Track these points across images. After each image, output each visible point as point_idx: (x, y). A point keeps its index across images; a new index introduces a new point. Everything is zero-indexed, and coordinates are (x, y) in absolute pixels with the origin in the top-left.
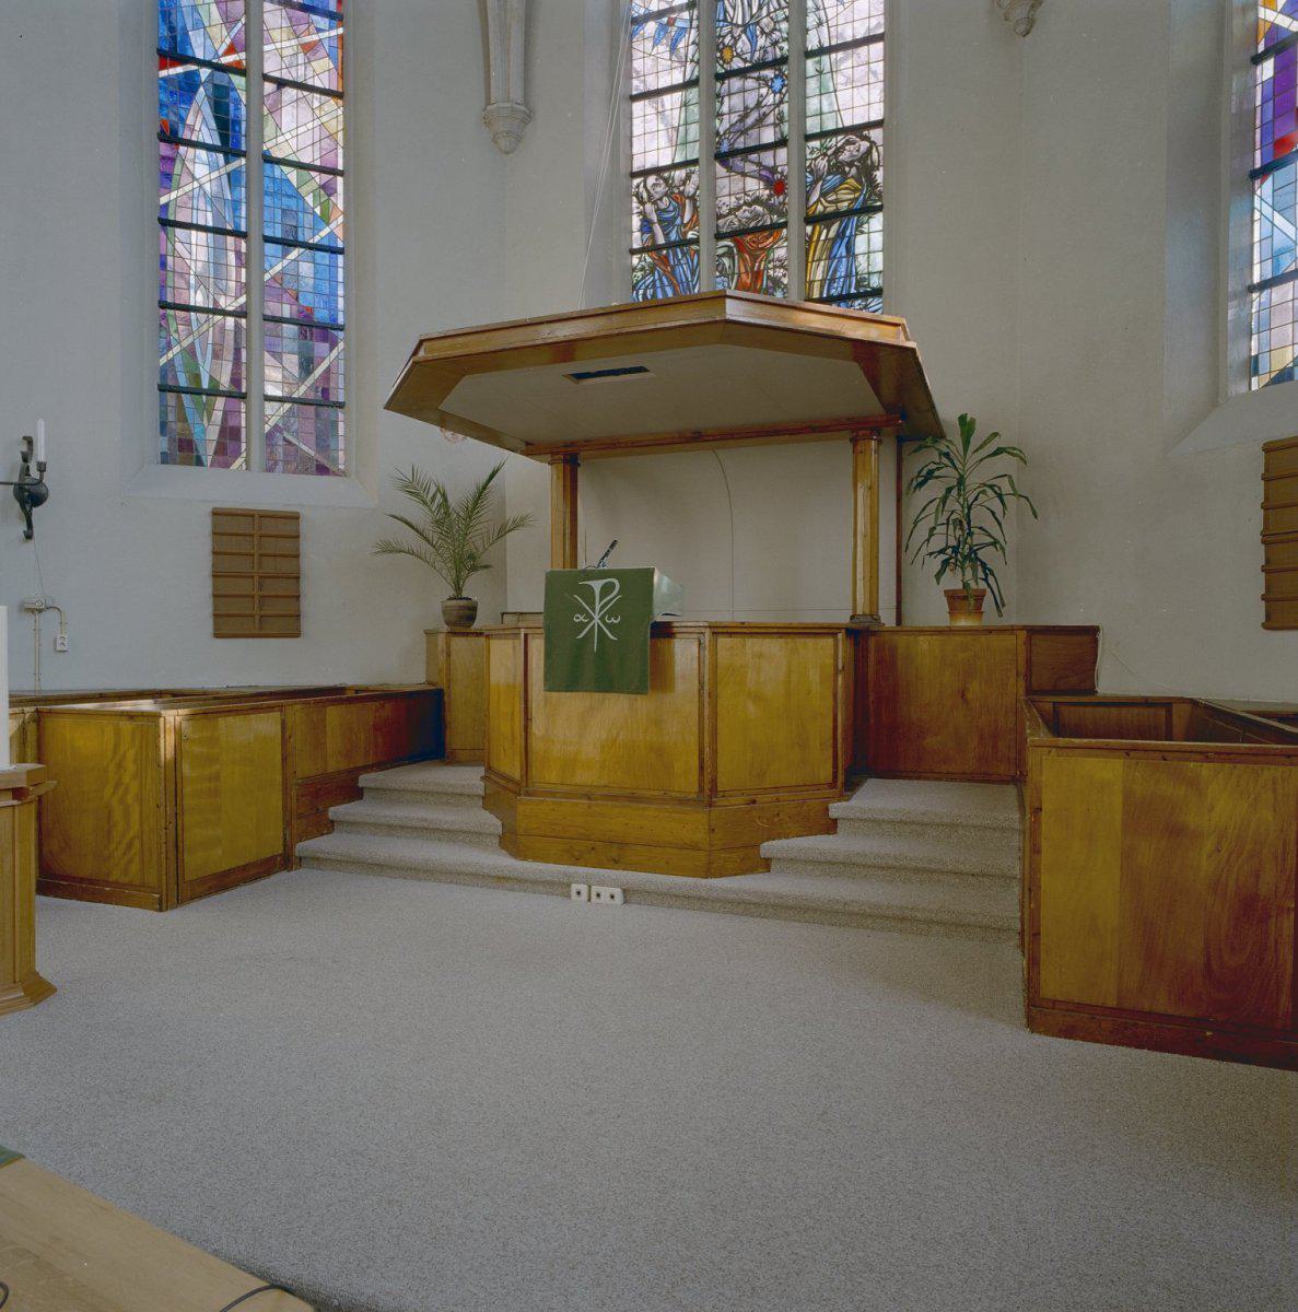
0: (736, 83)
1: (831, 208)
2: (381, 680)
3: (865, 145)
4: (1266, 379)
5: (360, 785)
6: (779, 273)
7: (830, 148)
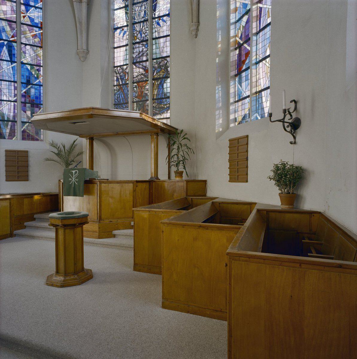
0: (137, 45)
1: (158, 77)
2: (50, 192)
3: (166, 61)
4: (238, 123)
5: (34, 217)
6: (147, 92)
7: (158, 62)
